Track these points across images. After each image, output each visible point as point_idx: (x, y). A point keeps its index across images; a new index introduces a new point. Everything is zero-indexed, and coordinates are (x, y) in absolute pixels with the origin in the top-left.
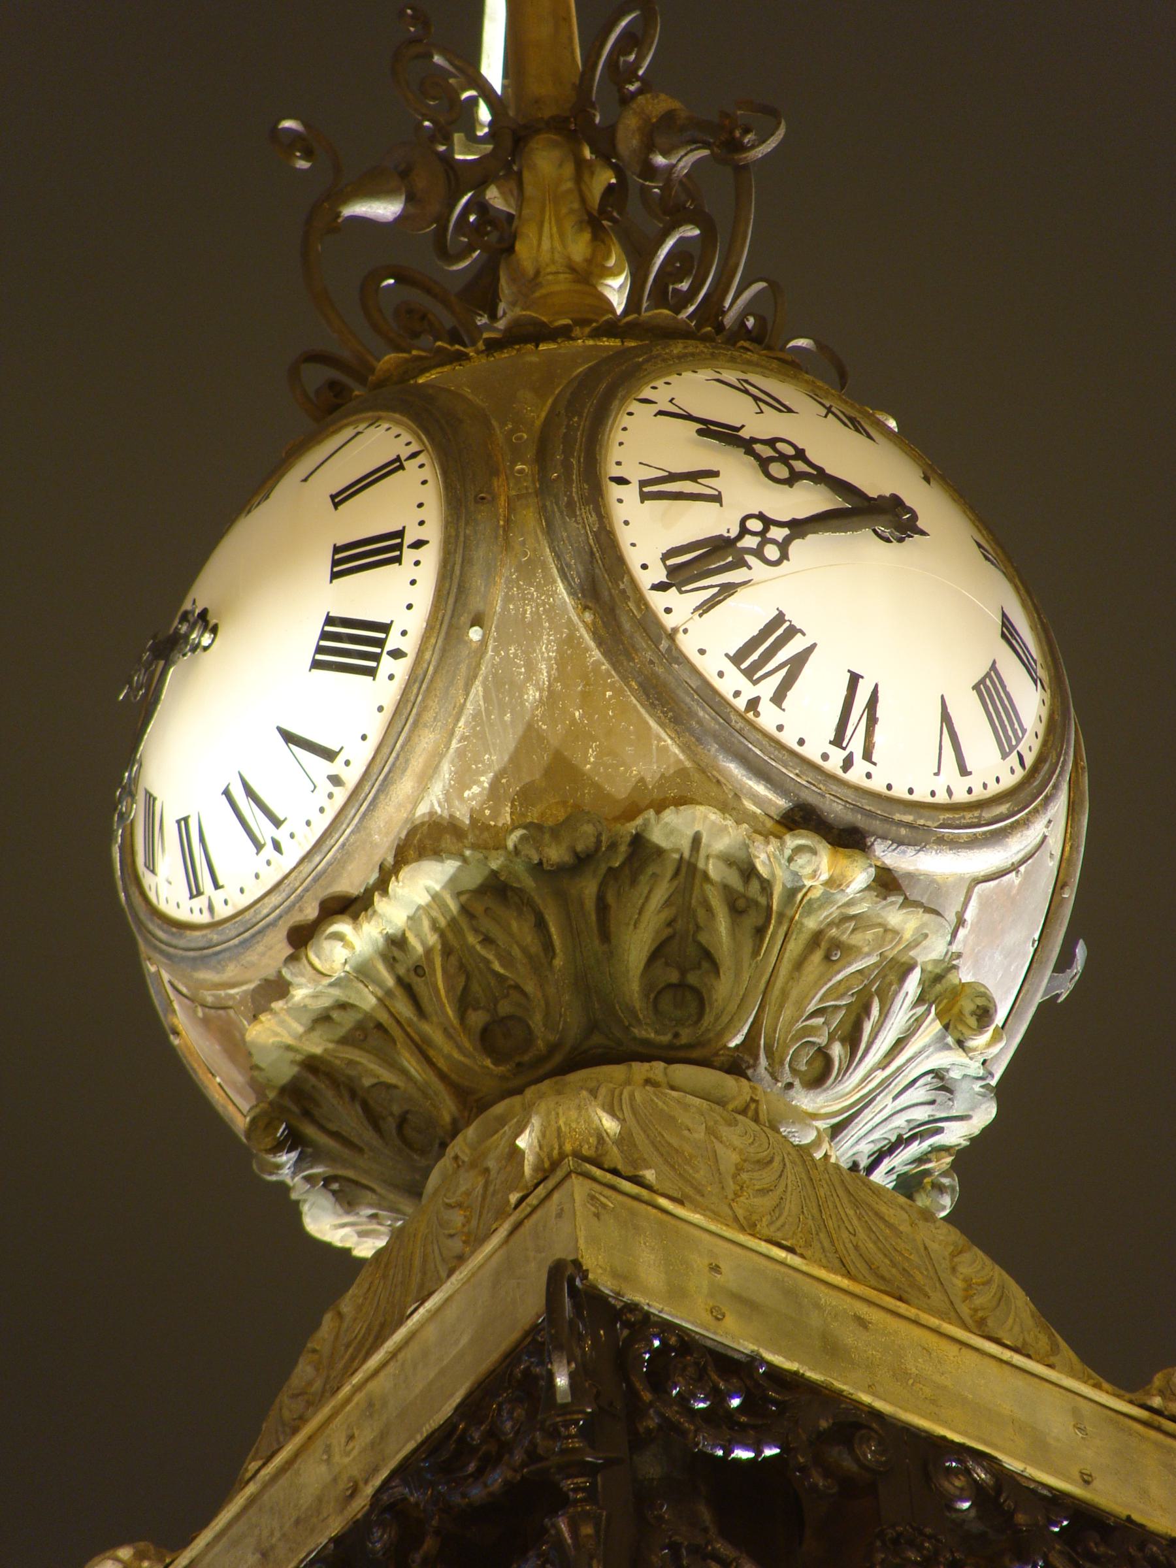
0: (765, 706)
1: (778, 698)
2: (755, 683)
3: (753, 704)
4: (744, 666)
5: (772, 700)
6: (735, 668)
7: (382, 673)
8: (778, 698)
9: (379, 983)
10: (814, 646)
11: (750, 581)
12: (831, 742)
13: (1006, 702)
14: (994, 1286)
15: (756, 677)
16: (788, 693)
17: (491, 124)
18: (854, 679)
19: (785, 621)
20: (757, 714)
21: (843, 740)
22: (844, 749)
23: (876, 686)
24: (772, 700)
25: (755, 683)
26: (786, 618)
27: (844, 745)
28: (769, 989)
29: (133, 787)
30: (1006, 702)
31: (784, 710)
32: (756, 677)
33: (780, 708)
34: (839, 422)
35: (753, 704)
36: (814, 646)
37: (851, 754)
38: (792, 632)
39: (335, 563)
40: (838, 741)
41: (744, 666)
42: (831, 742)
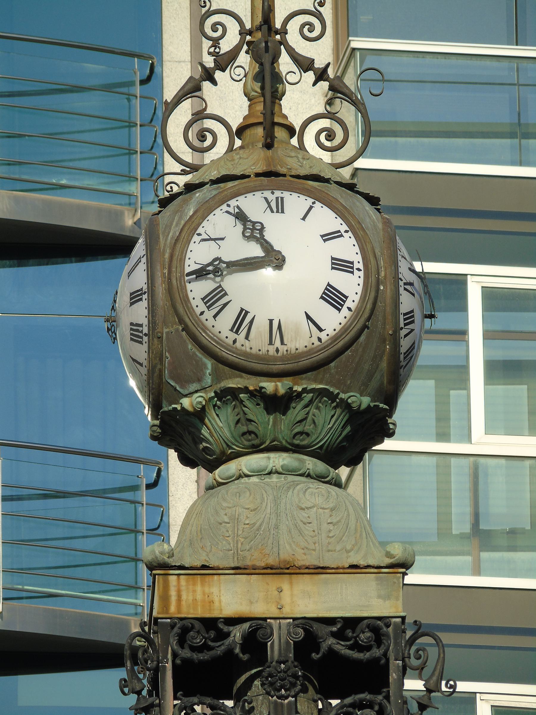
0: (281, 347)
1: (282, 343)
3: (277, 350)
7: (144, 342)
8: (282, 343)
18: (271, 321)
29: (351, 177)
35: (277, 350)
38: (247, 313)
39: (131, 299)
40: (271, 343)
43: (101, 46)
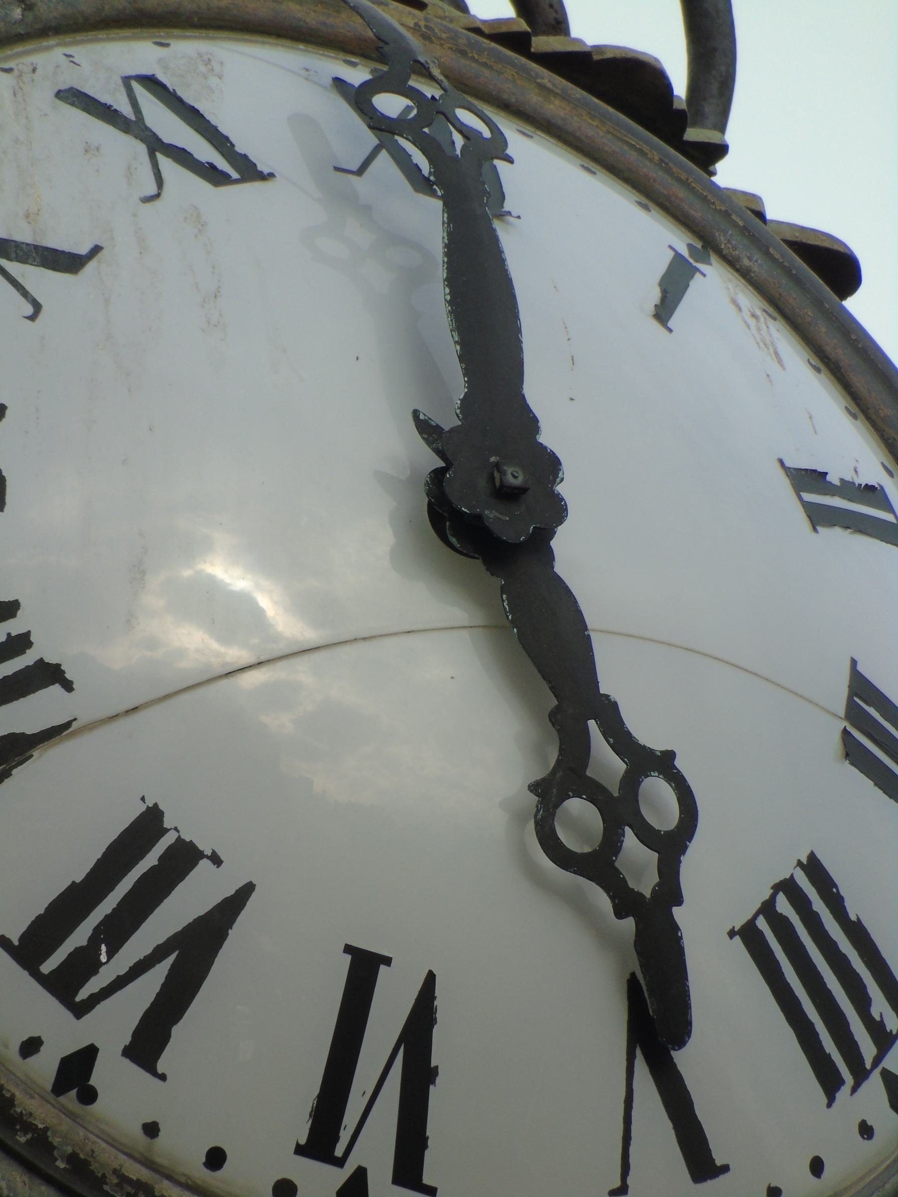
2: (80, 1010)
4: (47, 967)
5: (128, 1052)
6: (25, 974)
9: (450, 229)
10: (247, 890)
11: (68, 725)
12: (300, 1150)
13: (829, 1045)
14: (307, 73)
15: (83, 995)
16: (175, 1030)
17: (496, 456)
19: (167, 830)
20: (89, 1096)
21: (336, 1139)
22: (340, 1163)
23: (431, 978)
24: (128, 1052)
25: (80, 1010)
26: (167, 824)
27: (339, 1152)
28: (308, 651)
30: (829, 1045)
31: (163, 1077)
32: (83, 995)
33: (152, 1070)
34: (703, 1111)
36: (247, 890)
37: (361, 1174)
41: (47, 967)
42: (300, 1150)
43: (547, 139)
